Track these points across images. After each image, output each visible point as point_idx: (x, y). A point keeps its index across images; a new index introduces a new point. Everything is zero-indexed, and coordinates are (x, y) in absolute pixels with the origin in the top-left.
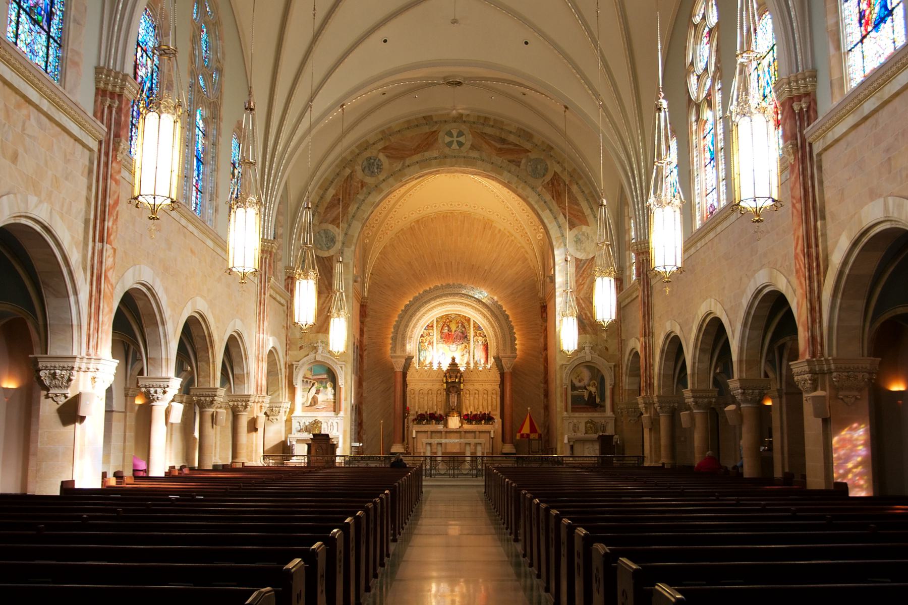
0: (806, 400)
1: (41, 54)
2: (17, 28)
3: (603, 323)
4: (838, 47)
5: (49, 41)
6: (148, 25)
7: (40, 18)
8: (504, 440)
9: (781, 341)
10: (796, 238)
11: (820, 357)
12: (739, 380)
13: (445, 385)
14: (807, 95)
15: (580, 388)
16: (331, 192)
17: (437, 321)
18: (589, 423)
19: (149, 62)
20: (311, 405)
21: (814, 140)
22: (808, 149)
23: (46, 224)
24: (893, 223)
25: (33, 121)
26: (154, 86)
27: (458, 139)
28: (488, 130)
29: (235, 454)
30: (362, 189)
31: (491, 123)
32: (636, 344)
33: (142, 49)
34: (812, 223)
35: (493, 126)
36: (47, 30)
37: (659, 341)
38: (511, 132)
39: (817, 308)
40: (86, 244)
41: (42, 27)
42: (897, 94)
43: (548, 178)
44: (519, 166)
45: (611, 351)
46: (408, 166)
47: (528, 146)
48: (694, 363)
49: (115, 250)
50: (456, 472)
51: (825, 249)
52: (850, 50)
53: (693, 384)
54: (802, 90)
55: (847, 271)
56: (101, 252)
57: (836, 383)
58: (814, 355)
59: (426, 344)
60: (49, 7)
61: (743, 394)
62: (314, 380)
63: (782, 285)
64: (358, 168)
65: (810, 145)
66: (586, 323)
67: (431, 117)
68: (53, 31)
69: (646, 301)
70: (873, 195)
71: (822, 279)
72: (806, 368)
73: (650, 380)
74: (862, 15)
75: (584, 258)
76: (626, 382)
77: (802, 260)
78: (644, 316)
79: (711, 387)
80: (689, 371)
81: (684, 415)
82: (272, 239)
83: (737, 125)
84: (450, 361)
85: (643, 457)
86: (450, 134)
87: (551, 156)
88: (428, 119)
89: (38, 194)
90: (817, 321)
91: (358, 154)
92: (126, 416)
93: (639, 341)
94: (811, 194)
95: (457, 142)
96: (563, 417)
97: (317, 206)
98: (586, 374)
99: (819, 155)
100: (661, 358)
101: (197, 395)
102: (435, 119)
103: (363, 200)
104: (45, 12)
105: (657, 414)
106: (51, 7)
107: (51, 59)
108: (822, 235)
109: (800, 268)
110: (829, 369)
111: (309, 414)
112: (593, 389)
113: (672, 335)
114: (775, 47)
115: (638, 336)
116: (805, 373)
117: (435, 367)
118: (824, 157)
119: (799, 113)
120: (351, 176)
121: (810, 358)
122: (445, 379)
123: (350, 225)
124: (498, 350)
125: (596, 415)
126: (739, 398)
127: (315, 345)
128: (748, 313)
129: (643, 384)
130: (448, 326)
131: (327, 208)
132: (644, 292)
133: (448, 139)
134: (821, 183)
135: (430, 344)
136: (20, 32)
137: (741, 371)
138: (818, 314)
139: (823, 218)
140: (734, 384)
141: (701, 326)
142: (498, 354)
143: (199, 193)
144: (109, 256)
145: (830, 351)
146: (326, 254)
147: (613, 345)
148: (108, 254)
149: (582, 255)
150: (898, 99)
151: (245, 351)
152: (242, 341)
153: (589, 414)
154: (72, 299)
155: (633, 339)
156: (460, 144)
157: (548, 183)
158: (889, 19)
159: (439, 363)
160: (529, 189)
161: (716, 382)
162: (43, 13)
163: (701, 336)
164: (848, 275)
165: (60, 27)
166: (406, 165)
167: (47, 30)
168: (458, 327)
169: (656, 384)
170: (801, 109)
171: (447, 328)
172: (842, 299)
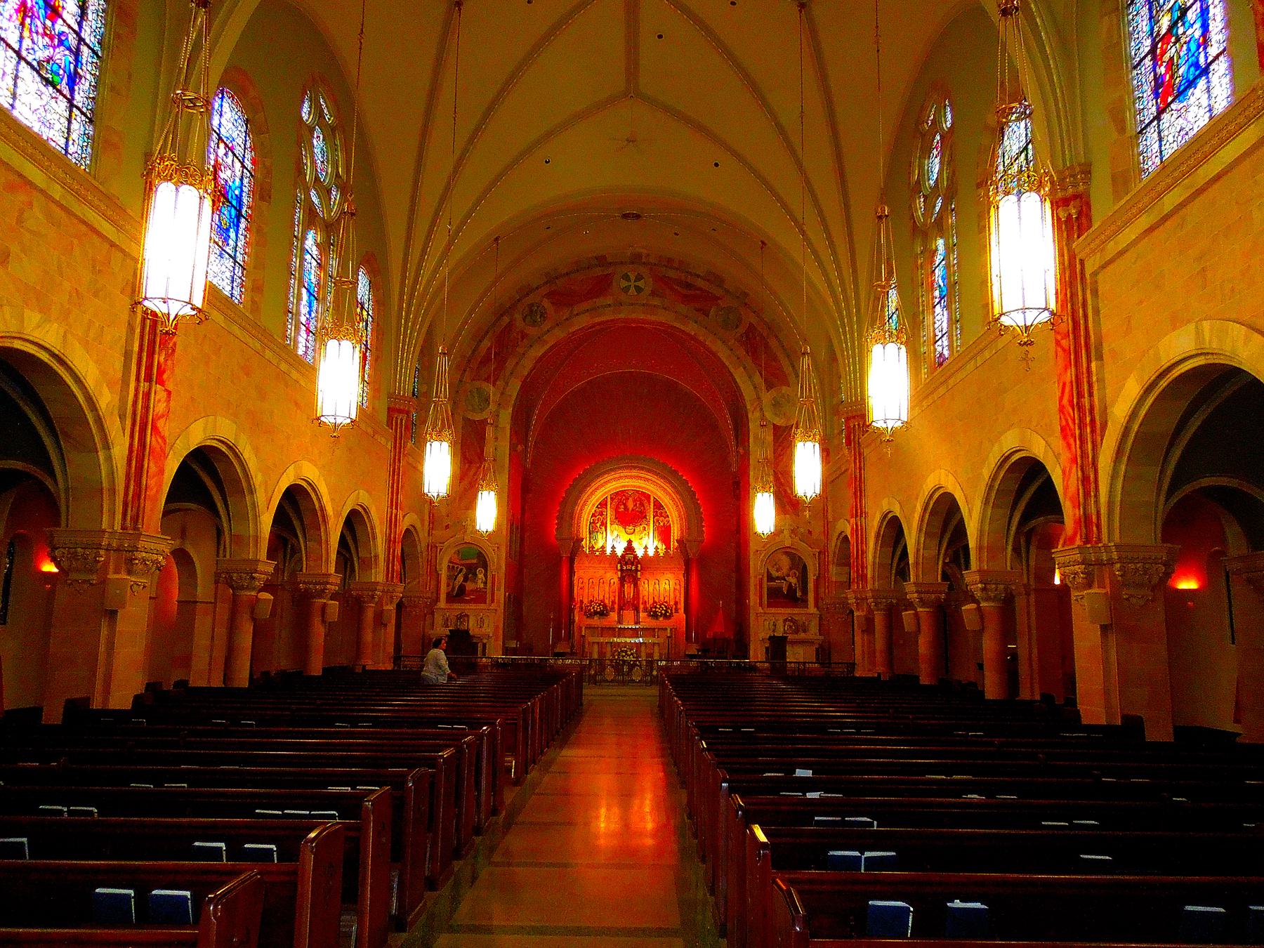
0: (1077, 600)
1: (57, 126)
2: (15, 85)
3: (804, 498)
4: (1121, 126)
5: (71, 112)
6: (236, 117)
7: (57, 79)
8: (688, 638)
9: (1033, 523)
10: (1061, 384)
11: (1097, 543)
12: (979, 571)
13: (619, 573)
14: (1075, 197)
15: (778, 578)
16: (486, 343)
17: (611, 498)
18: (789, 621)
19: (238, 165)
20: (458, 595)
21: (1088, 255)
22: (1078, 266)
23: (57, 352)
24: (1209, 356)
25: (37, 211)
26: (244, 194)
27: (636, 284)
28: (672, 274)
29: (209, 682)
30: (522, 341)
31: (676, 265)
32: (845, 527)
33: (226, 146)
34: (1085, 365)
35: (677, 269)
36: (69, 96)
37: (874, 523)
38: (698, 276)
39: (1092, 476)
40: (125, 383)
41: (60, 92)
42: (1218, 177)
43: (741, 330)
44: (708, 316)
45: (815, 536)
46: (577, 314)
47: (718, 292)
48: (918, 550)
49: (169, 393)
50: (627, 678)
51: (1103, 400)
52: (1141, 132)
53: (917, 576)
54: (1070, 191)
55: (1136, 427)
56: (147, 396)
57: (1119, 578)
58: (1087, 540)
59: (598, 525)
60: (72, 66)
61: (984, 589)
62: (462, 565)
63: (1038, 449)
64: (518, 316)
65: (1082, 262)
66: (787, 501)
67: (604, 257)
68: (79, 99)
69: (858, 476)
70: (1176, 322)
71: (1099, 438)
72: (1078, 557)
73: (862, 571)
74: (1158, 81)
75: (783, 425)
76: (834, 572)
77: (1069, 414)
78: (855, 493)
79: (940, 581)
80: (911, 560)
81: (907, 615)
82: (410, 395)
83: (998, 208)
84: (625, 545)
85: (853, 665)
86: (626, 278)
87: (746, 304)
88: (601, 260)
89: (44, 310)
90: (1092, 494)
91: (519, 300)
92: (215, 607)
93: (849, 522)
94: (1082, 327)
95: (629, 280)
96: (757, 614)
97: (469, 361)
98: (785, 562)
99: (1095, 274)
100: (876, 543)
101: (304, 583)
102: (609, 260)
103: (524, 354)
104: (65, 72)
105: (870, 611)
106: (76, 66)
107: (74, 136)
108: (1098, 380)
109: (1068, 424)
110: (1110, 559)
111: (456, 606)
112: (793, 581)
113: (890, 516)
114: (1030, 146)
115: (848, 517)
116: (336, 585)
117: (608, 551)
118: (1100, 277)
119: (1066, 221)
120: (510, 325)
121: (1082, 543)
122: (619, 565)
123: (507, 383)
124: (682, 533)
125: (796, 611)
126: (978, 594)
127: (464, 524)
128: (991, 487)
129: (853, 575)
130: (625, 505)
131: (481, 362)
132: (855, 463)
133: (624, 284)
134: (1097, 311)
135: (602, 524)
136: (19, 91)
137: (980, 559)
138: (1093, 485)
139: (1100, 357)
140: (971, 578)
141: (927, 504)
142: (682, 537)
143: (311, 334)
144: (159, 401)
145: (1111, 534)
146: (478, 417)
147: (817, 528)
148: (157, 398)
149: (782, 421)
150: (1216, 186)
151: (372, 529)
152: (368, 517)
153: (789, 611)
154: (101, 455)
155: (842, 520)
156: (638, 289)
157: (742, 336)
158: (1202, 83)
159: (613, 547)
160: (719, 342)
161: (945, 576)
162: (61, 72)
163: (927, 516)
164: (1137, 433)
165: (91, 96)
166: (575, 313)
167: (69, 96)
168: (636, 504)
169: (869, 576)
170: (1070, 216)
171: (623, 506)
172: (1127, 465)
